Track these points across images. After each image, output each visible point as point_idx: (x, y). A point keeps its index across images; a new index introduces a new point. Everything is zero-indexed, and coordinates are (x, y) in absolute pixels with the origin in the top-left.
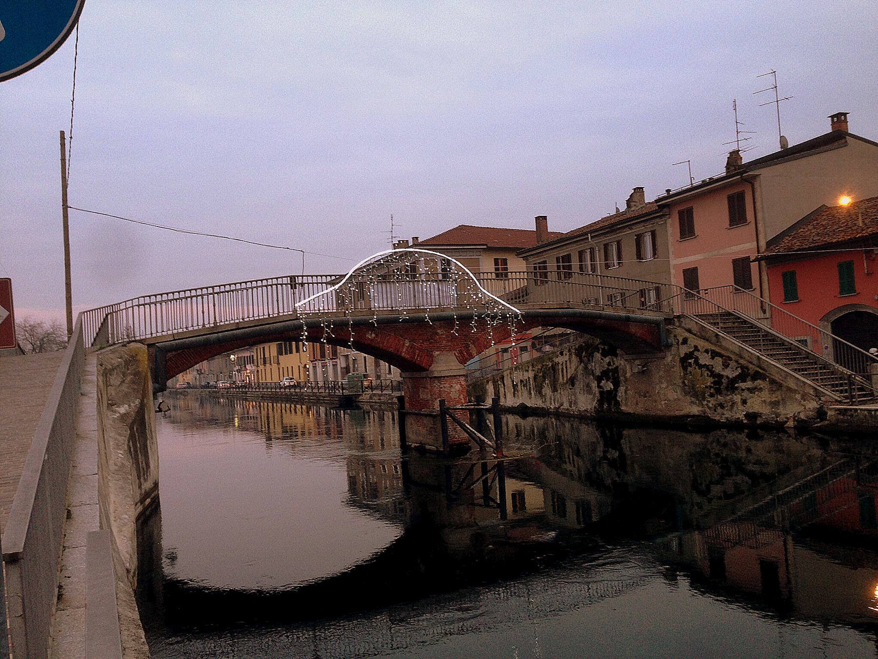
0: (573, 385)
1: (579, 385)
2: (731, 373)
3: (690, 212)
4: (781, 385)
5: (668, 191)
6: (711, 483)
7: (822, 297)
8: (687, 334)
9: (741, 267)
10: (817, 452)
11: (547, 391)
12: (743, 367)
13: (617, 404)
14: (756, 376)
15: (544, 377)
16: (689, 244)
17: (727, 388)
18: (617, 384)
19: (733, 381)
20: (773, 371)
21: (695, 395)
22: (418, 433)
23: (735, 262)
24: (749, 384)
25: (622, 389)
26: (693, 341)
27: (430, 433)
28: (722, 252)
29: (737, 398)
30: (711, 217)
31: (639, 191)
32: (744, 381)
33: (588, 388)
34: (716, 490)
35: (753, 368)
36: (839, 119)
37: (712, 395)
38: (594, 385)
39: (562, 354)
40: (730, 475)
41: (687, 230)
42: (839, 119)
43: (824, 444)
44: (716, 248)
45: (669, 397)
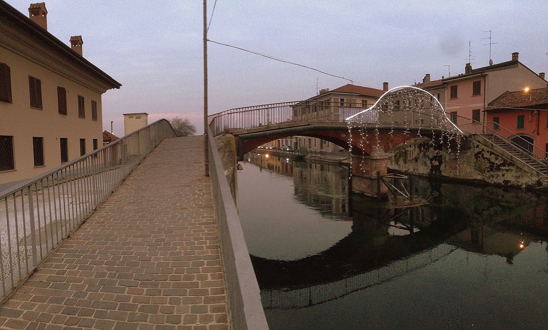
0: (417, 161)
1: (420, 162)
2: (498, 162)
3: (456, 87)
4: (521, 169)
5: (443, 77)
6: (484, 210)
7: (508, 129)
8: (478, 143)
9: (476, 114)
10: (535, 199)
11: (401, 162)
12: (504, 160)
13: (440, 172)
14: (510, 164)
15: (400, 156)
16: (454, 101)
17: (496, 169)
18: (440, 163)
19: (500, 165)
20: (518, 162)
21: (480, 171)
22: (359, 186)
23: (474, 111)
24: (507, 168)
25: (443, 166)
26: (482, 147)
27: (369, 188)
28: (462, 107)
29: (500, 174)
30: (465, 90)
31: (428, 75)
32: (504, 166)
33: (425, 164)
34: (486, 213)
35: (509, 161)
36: (515, 55)
37: (488, 171)
38: (428, 162)
39: (410, 146)
40: (493, 206)
41: (454, 95)
42: (515, 55)
43: (538, 196)
44: (467, 103)
45: (467, 170)
